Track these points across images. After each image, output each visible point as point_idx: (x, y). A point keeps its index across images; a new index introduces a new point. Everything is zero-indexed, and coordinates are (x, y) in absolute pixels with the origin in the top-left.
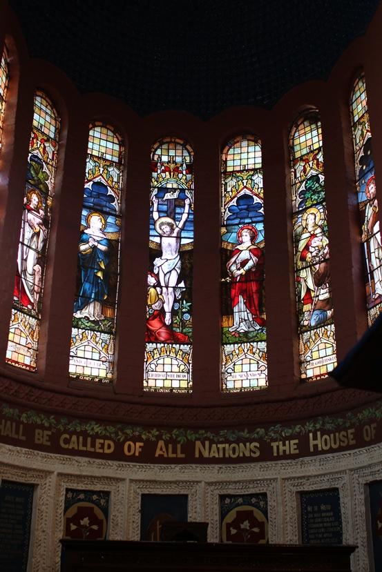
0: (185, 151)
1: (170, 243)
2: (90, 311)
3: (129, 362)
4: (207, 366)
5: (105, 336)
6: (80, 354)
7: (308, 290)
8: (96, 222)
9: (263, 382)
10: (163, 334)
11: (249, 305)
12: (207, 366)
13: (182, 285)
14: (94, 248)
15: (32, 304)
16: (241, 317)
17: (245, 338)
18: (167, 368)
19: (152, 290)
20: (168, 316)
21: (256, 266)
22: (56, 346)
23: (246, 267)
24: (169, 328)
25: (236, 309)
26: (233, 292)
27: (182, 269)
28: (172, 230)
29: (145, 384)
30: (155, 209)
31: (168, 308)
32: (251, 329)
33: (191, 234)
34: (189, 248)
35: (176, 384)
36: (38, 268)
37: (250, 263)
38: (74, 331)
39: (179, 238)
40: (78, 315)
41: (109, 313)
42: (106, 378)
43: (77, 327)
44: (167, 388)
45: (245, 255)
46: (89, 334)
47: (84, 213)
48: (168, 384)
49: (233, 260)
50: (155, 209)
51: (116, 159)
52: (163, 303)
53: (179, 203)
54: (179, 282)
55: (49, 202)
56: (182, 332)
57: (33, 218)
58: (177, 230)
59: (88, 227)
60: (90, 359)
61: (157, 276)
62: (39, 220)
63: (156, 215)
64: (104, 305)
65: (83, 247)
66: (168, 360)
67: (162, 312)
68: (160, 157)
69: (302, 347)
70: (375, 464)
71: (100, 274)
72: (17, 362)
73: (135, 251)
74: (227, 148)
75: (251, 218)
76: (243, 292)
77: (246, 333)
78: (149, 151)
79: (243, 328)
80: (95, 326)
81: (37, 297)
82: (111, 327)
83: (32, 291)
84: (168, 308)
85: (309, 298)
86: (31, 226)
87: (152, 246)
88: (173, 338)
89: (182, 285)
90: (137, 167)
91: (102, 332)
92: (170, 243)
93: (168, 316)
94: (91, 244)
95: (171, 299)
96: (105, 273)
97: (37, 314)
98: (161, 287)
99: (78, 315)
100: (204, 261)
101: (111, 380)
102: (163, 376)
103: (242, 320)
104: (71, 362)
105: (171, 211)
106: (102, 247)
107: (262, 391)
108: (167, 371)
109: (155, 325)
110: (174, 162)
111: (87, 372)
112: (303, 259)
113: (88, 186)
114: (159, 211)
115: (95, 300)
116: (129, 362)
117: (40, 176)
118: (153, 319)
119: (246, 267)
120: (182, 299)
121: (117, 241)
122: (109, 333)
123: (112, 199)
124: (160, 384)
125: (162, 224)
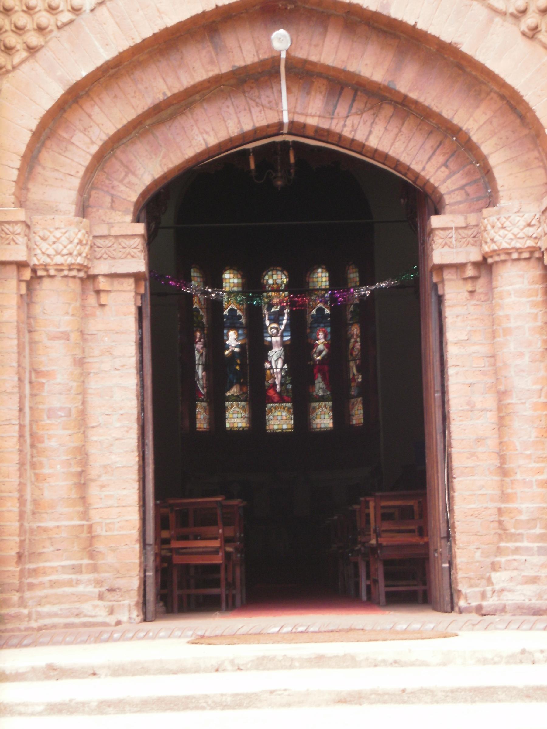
0: (283, 275)
1: (276, 336)
2: (234, 391)
3: (257, 416)
4: (302, 416)
5: (244, 403)
6: (231, 416)
7: (354, 375)
8: (232, 335)
9: (331, 425)
10: (276, 398)
11: (324, 379)
12: (302, 416)
13: (286, 366)
14: (233, 351)
15: (203, 395)
16: (320, 387)
17: (322, 399)
18: (279, 418)
19: (268, 372)
20: (278, 387)
21: (327, 355)
22: (218, 415)
23: (322, 355)
24: (280, 394)
25: (316, 382)
26: (315, 371)
27: (285, 356)
28: (278, 331)
29: (267, 428)
30: (266, 318)
31: (277, 382)
32: (325, 394)
33: (289, 334)
34: (289, 343)
35: (285, 427)
36: (204, 373)
37: (324, 353)
38: (227, 404)
39: (282, 336)
40: (228, 394)
41: (244, 389)
42: (246, 427)
43: (228, 401)
44: (280, 429)
45: (321, 347)
46: (235, 403)
47: (225, 331)
48: (280, 427)
49: (314, 350)
50: (266, 318)
51: (240, 289)
52: (275, 379)
53: (281, 313)
54: (283, 365)
55: (205, 332)
56: (287, 396)
57: (199, 346)
58: (280, 331)
59: (228, 339)
60: (236, 418)
61: (270, 363)
62: (201, 346)
63: (267, 323)
64: (242, 385)
65: (227, 353)
66: (279, 413)
67: (274, 385)
68: (267, 281)
69: (351, 406)
70: (474, 134)
71: (237, 368)
72: (201, 428)
73: (256, 347)
74: (309, 273)
75: (324, 323)
76: (320, 371)
77: (322, 396)
78: (260, 277)
79: (321, 393)
80: (237, 399)
81: (205, 390)
82: (247, 397)
83: (203, 388)
84: (277, 382)
85: (354, 379)
86: (199, 352)
87: (266, 343)
88: (282, 400)
89: (286, 366)
90: (253, 286)
91: (242, 401)
92: (276, 336)
93: (278, 387)
94: (230, 350)
95: (279, 376)
96: (240, 365)
97: (207, 400)
98: (273, 369)
99: (228, 394)
100: (297, 351)
101: (249, 428)
102: (277, 422)
103: (320, 388)
104: (227, 421)
105: (276, 318)
106: (236, 350)
107: (333, 404)
108: (280, 420)
109: (271, 393)
110: (277, 284)
111: (235, 425)
112: (351, 354)
113: (226, 313)
114: (269, 319)
115: (237, 383)
116: (257, 416)
117: (199, 318)
118: (270, 389)
119: (322, 355)
120: (286, 376)
121: (245, 344)
122: (245, 400)
123: (240, 317)
124: (276, 427)
125: (272, 328)
